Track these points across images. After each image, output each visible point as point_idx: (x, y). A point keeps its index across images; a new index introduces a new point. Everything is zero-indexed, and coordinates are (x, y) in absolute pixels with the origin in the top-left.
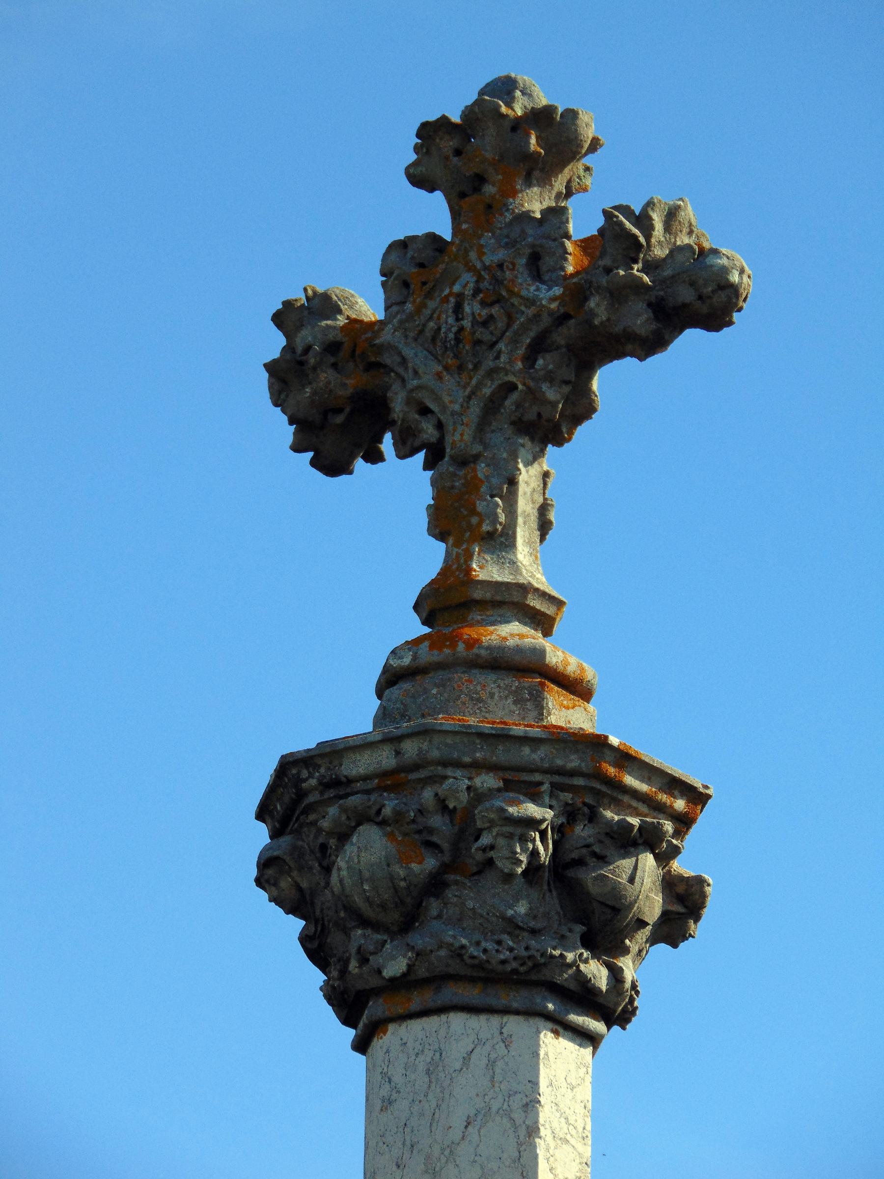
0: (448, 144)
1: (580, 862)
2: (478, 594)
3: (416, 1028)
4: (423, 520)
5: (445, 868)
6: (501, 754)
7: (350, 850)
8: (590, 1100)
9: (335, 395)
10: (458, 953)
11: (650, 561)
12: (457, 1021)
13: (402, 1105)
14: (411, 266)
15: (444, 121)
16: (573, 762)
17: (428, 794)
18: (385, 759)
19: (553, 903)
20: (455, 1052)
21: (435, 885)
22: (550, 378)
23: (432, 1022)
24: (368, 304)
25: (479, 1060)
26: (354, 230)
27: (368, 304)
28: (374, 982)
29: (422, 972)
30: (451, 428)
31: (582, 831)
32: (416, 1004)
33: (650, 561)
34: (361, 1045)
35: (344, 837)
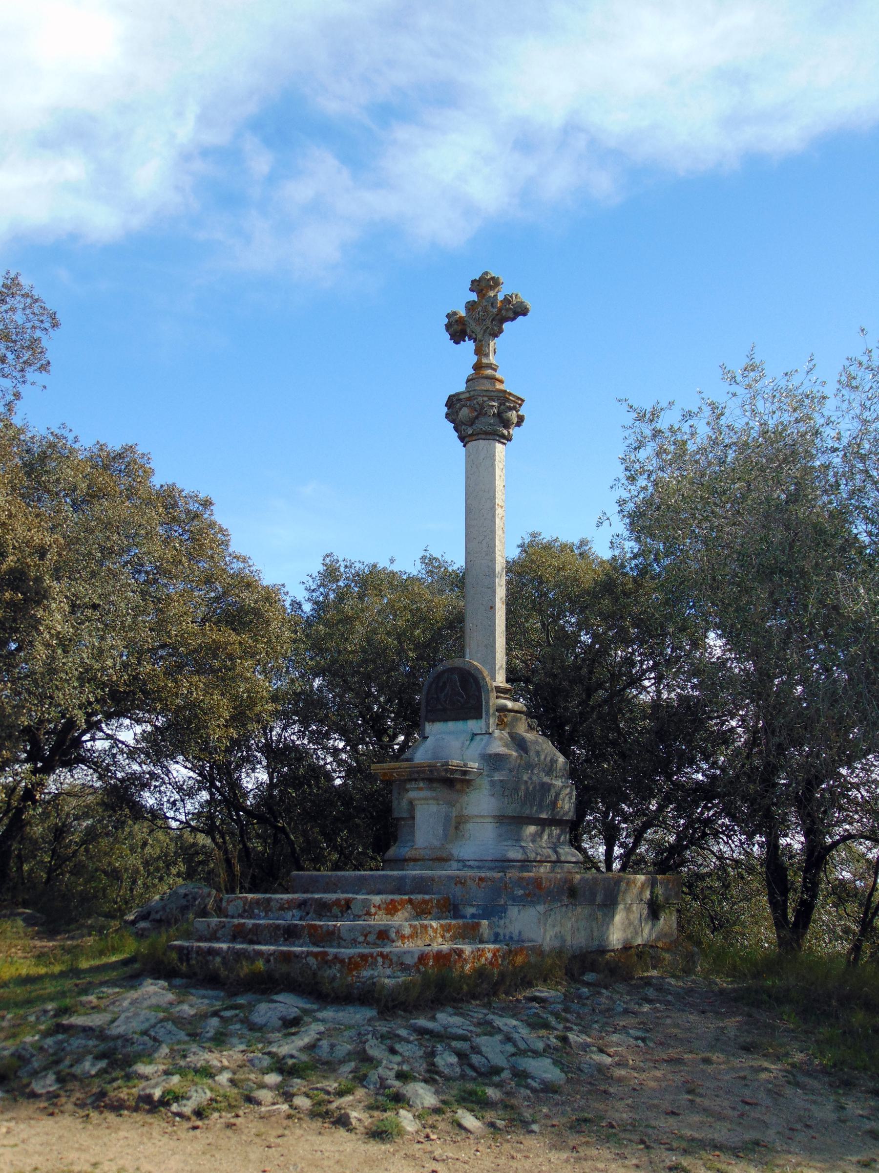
6: (488, 394)
12: (481, 441)
14: (471, 306)
18: (467, 395)
21: (477, 417)
24: (463, 313)
26: (459, 300)
27: (463, 313)
35: (460, 409)
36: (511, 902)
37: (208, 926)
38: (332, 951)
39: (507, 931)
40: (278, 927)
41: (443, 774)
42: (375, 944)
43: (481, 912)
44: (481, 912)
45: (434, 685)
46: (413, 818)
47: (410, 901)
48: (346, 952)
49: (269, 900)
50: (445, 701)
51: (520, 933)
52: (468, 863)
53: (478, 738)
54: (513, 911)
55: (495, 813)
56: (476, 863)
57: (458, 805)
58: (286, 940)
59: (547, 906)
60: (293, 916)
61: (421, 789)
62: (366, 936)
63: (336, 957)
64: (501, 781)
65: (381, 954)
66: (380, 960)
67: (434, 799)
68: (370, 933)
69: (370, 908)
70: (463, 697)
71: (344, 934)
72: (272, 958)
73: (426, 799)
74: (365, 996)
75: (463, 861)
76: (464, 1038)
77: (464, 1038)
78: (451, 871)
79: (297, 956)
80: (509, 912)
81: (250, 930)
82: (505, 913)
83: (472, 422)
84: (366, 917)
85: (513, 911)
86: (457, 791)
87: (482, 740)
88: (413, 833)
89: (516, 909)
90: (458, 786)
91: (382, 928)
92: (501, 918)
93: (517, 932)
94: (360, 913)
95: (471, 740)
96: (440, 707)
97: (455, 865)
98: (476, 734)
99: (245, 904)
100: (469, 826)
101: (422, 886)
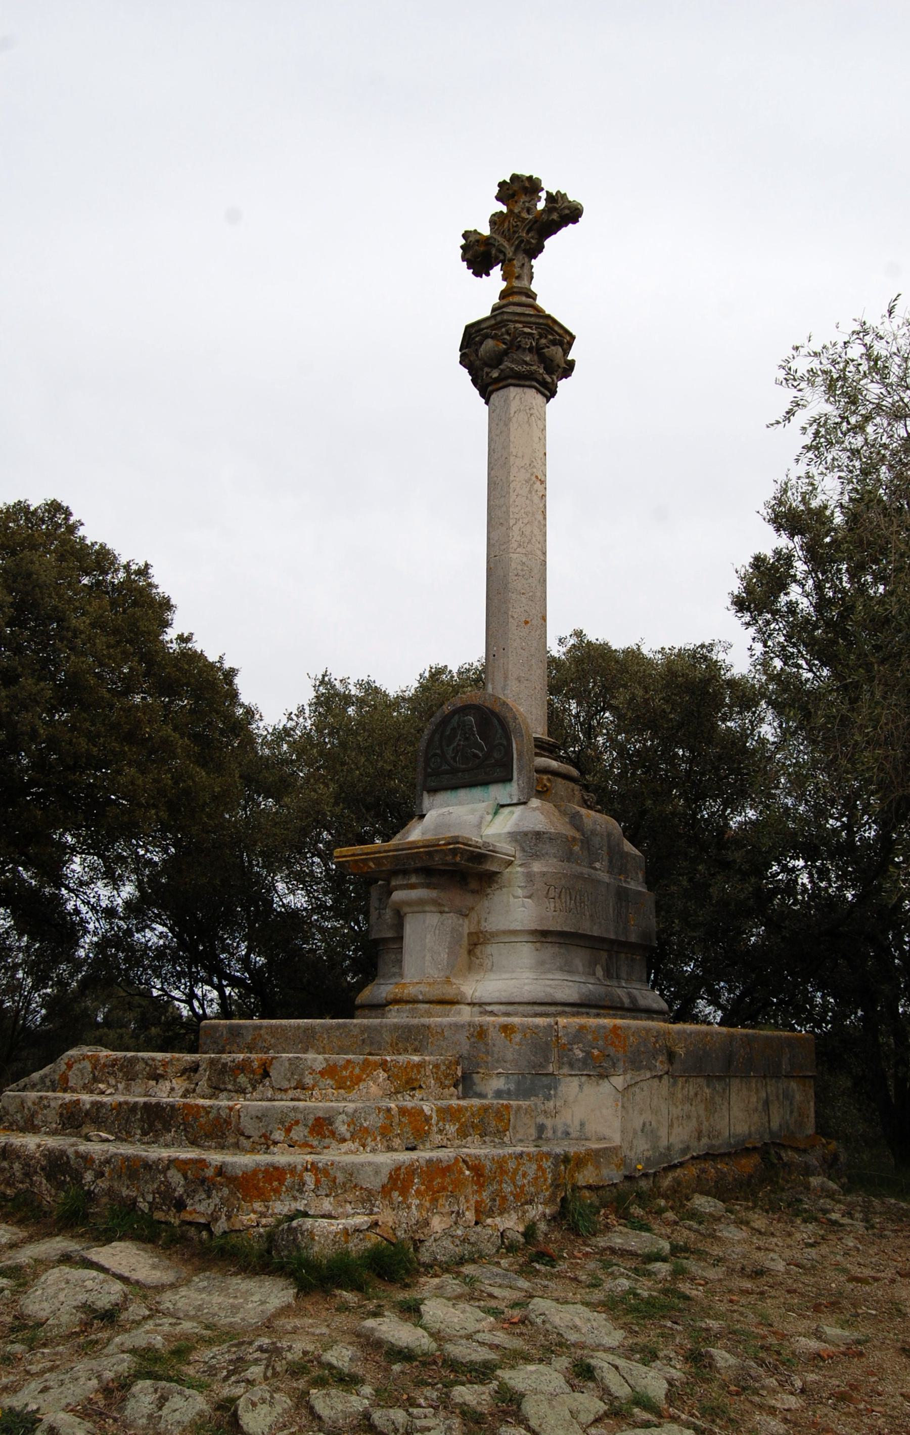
0: (506, 187)
1: (543, 348)
2: (515, 290)
3: (501, 393)
4: (501, 278)
5: (508, 349)
6: (522, 319)
7: (483, 346)
8: (470, 806)
9: (479, 255)
10: (512, 369)
11: (559, 278)
12: (512, 389)
13: (498, 410)
14: (496, 221)
15: (504, 182)
16: (541, 321)
17: (503, 330)
18: (493, 322)
19: (536, 358)
20: (512, 395)
21: (505, 353)
22: (532, 238)
23: (505, 390)
24: (486, 231)
25: (517, 397)
26: (481, 212)
27: (486, 231)
28: (490, 381)
29: (503, 376)
30: (486, 823)
31: (543, 341)
32: (501, 385)
33: (559, 278)
34: (487, 403)
35: (481, 343)
36: (566, 1070)
37: (22, 1102)
38: (215, 1157)
39: (559, 1122)
40: (134, 1108)
41: (449, 858)
42: (306, 1145)
43: (512, 1087)
44: (512, 1087)
45: (437, 737)
46: (400, 938)
47: (384, 1065)
48: (243, 1161)
49: (132, 1061)
50: (454, 758)
51: (582, 1125)
52: (489, 1008)
53: (506, 811)
54: (570, 1087)
55: (533, 926)
56: (503, 1008)
57: (473, 915)
58: (145, 1133)
59: (628, 1076)
60: (172, 1089)
61: (412, 887)
62: (288, 1130)
63: (220, 1170)
64: (544, 874)
65: (313, 1168)
66: (309, 1178)
67: (435, 902)
68: (297, 1123)
69: (302, 1075)
70: (482, 750)
71: (247, 1125)
72: (107, 1169)
73: (421, 902)
74: (276, 1256)
75: (481, 1004)
76: (481, 1372)
77: (481, 1372)
78: (465, 1015)
79: (148, 1166)
80: (562, 1089)
81: (87, 1113)
82: (556, 1088)
83: (497, 360)
84: (298, 1093)
85: (570, 1087)
86: (473, 892)
87: (512, 813)
88: (399, 962)
89: (575, 1081)
90: (473, 885)
91: (321, 1114)
92: (548, 1098)
93: (577, 1123)
94: (286, 1085)
95: (496, 813)
96: (445, 767)
97: (466, 1009)
98: (503, 806)
99: (95, 1067)
100: (491, 949)
101: (413, 1039)
